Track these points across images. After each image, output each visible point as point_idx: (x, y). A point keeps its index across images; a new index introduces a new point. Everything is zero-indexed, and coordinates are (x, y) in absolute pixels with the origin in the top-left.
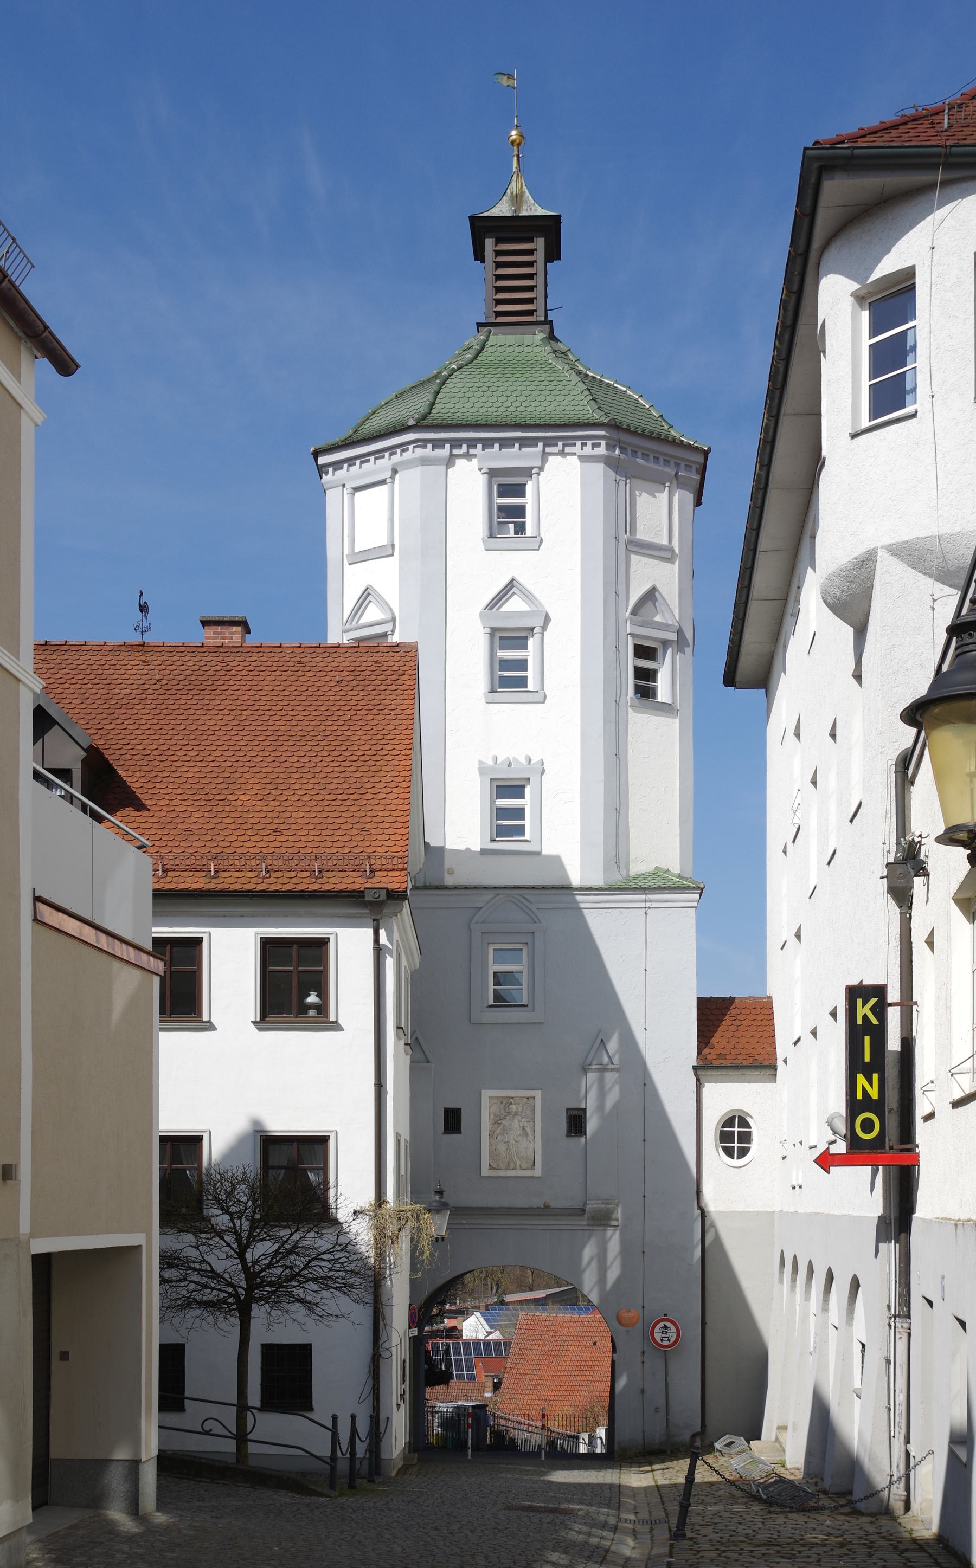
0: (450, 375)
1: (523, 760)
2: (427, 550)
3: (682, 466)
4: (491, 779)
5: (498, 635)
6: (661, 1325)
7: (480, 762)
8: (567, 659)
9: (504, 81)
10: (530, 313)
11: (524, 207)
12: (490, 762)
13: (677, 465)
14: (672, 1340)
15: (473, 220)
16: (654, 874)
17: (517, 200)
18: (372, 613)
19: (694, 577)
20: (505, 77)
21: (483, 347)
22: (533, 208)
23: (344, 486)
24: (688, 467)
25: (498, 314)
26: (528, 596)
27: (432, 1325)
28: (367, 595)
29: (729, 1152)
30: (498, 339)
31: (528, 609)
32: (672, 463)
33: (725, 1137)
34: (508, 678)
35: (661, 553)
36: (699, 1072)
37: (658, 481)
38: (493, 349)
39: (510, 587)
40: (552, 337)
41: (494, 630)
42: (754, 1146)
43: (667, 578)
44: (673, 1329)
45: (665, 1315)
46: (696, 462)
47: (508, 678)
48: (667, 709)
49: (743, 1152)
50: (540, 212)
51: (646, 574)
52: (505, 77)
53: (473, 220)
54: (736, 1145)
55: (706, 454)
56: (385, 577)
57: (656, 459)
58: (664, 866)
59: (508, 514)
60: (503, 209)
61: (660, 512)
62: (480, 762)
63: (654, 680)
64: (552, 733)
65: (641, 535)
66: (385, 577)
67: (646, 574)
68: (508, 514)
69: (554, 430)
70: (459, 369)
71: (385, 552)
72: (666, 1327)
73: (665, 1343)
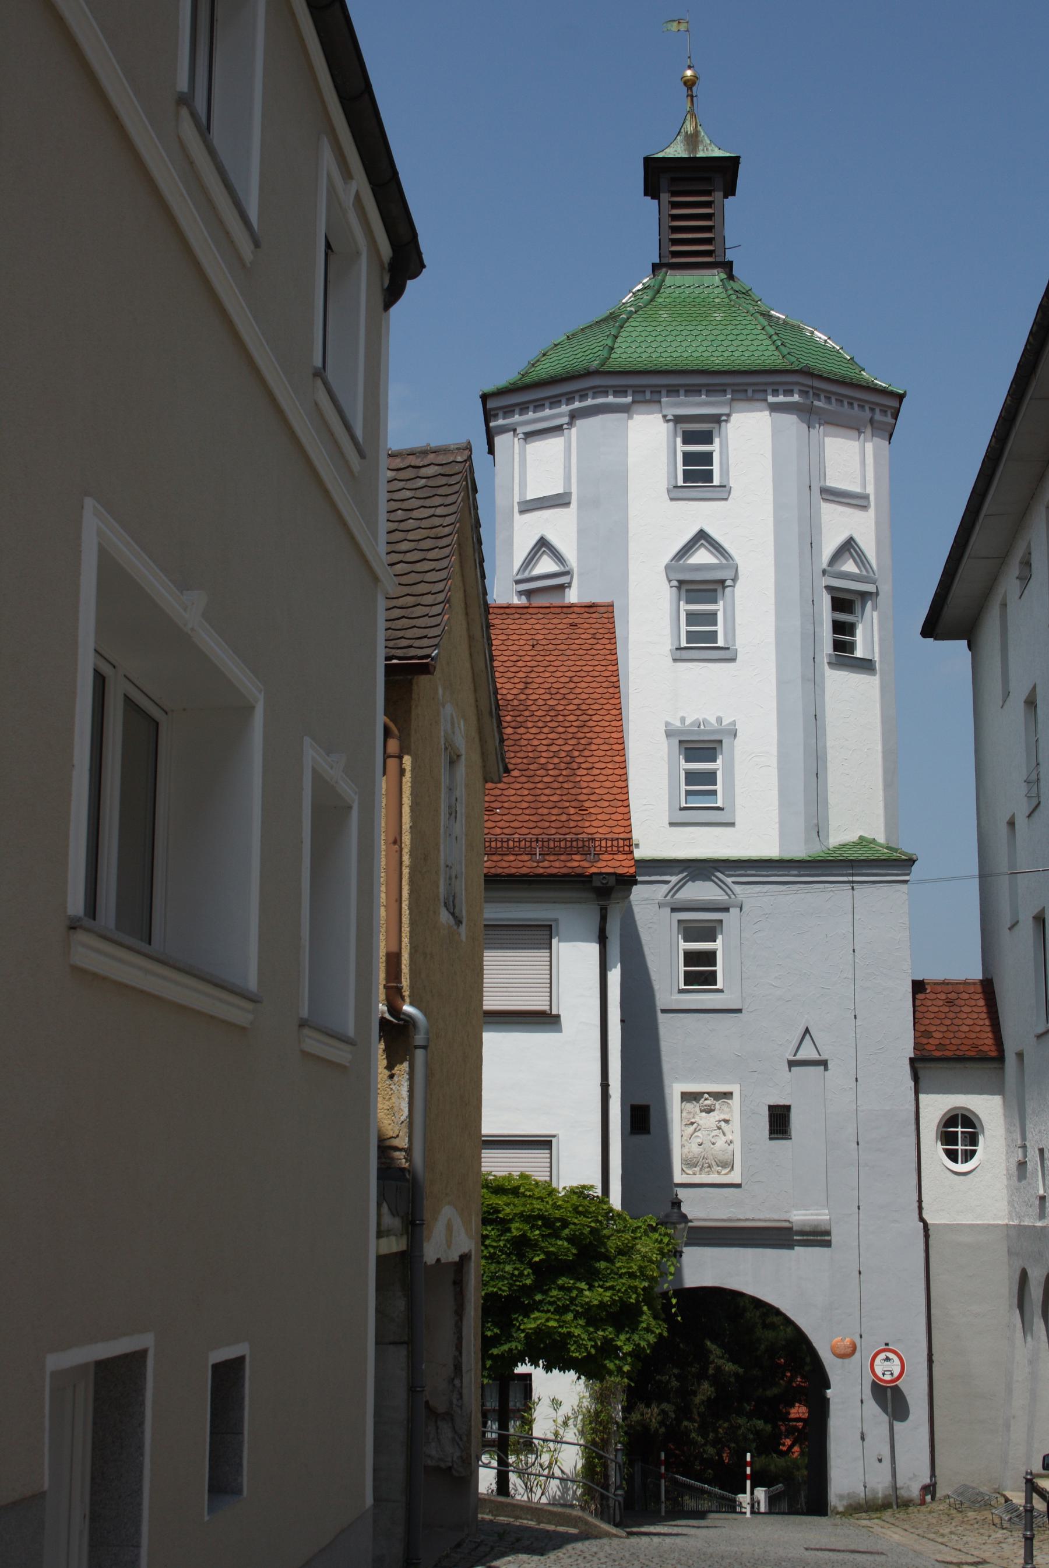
0: (628, 318)
1: (713, 721)
2: (602, 496)
3: (877, 411)
4: (680, 742)
5: (684, 588)
6: (882, 1356)
7: (667, 724)
8: (757, 612)
9: (674, 27)
10: (709, 253)
11: (701, 148)
12: (678, 724)
13: (872, 410)
14: (896, 1374)
15: (649, 162)
16: (858, 844)
17: (693, 140)
18: (546, 565)
19: (897, 527)
20: (675, 24)
21: (660, 287)
22: (710, 150)
23: (515, 430)
24: (884, 412)
25: (675, 254)
26: (717, 548)
27: (619, 1331)
28: (543, 545)
29: (952, 1155)
30: (673, 278)
31: (715, 561)
32: (867, 408)
33: (947, 1138)
34: (701, 641)
35: (855, 501)
36: (918, 1065)
37: (855, 427)
38: (668, 291)
39: (702, 537)
40: (731, 277)
41: (681, 583)
42: (980, 1149)
43: (862, 527)
44: (897, 1361)
45: (887, 1344)
46: (891, 407)
47: (701, 641)
48: (866, 666)
49: (969, 1155)
50: (717, 153)
51: (837, 524)
52: (675, 24)
53: (649, 162)
54: (960, 1147)
55: (901, 397)
56: (561, 528)
57: (851, 404)
58: (868, 835)
59: (697, 473)
60: (677, 150)
61: (850, 458)
62: (667, 724)
63: (852, 633)
64: (745, 694)
65: (831, 483)
66: (561, 528)
67: (837, 524)
68: (697, 473)
69: (746, 384)
70: (636, 312)
71: (559, 501)
72: (887, 1359)
73: (888, 1377)
